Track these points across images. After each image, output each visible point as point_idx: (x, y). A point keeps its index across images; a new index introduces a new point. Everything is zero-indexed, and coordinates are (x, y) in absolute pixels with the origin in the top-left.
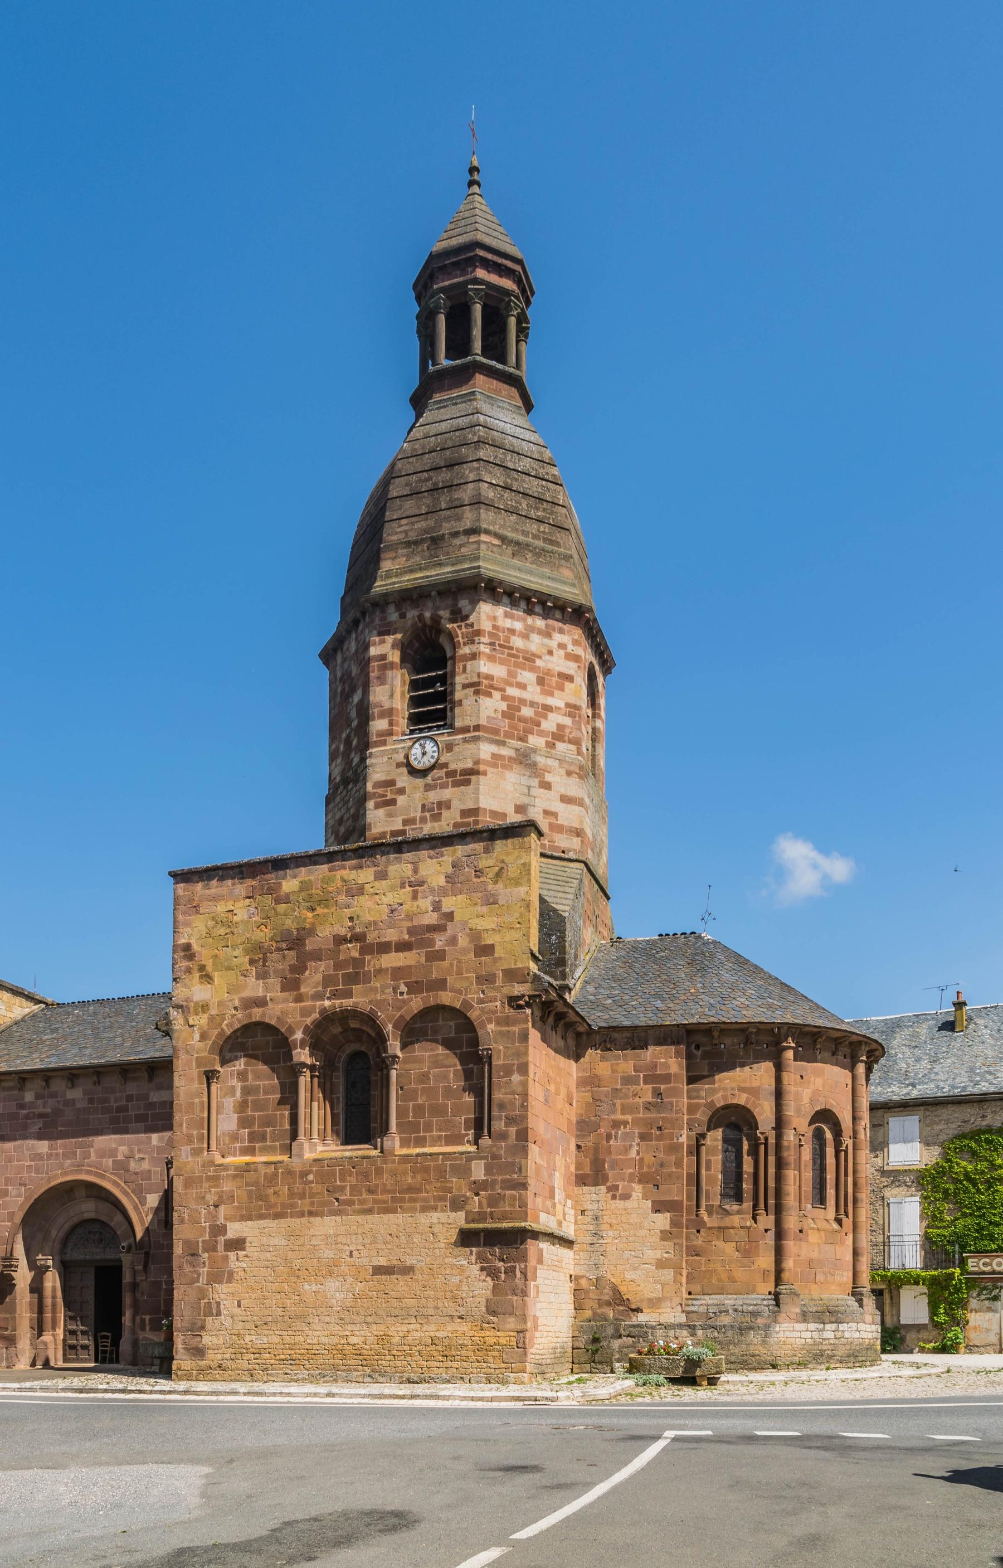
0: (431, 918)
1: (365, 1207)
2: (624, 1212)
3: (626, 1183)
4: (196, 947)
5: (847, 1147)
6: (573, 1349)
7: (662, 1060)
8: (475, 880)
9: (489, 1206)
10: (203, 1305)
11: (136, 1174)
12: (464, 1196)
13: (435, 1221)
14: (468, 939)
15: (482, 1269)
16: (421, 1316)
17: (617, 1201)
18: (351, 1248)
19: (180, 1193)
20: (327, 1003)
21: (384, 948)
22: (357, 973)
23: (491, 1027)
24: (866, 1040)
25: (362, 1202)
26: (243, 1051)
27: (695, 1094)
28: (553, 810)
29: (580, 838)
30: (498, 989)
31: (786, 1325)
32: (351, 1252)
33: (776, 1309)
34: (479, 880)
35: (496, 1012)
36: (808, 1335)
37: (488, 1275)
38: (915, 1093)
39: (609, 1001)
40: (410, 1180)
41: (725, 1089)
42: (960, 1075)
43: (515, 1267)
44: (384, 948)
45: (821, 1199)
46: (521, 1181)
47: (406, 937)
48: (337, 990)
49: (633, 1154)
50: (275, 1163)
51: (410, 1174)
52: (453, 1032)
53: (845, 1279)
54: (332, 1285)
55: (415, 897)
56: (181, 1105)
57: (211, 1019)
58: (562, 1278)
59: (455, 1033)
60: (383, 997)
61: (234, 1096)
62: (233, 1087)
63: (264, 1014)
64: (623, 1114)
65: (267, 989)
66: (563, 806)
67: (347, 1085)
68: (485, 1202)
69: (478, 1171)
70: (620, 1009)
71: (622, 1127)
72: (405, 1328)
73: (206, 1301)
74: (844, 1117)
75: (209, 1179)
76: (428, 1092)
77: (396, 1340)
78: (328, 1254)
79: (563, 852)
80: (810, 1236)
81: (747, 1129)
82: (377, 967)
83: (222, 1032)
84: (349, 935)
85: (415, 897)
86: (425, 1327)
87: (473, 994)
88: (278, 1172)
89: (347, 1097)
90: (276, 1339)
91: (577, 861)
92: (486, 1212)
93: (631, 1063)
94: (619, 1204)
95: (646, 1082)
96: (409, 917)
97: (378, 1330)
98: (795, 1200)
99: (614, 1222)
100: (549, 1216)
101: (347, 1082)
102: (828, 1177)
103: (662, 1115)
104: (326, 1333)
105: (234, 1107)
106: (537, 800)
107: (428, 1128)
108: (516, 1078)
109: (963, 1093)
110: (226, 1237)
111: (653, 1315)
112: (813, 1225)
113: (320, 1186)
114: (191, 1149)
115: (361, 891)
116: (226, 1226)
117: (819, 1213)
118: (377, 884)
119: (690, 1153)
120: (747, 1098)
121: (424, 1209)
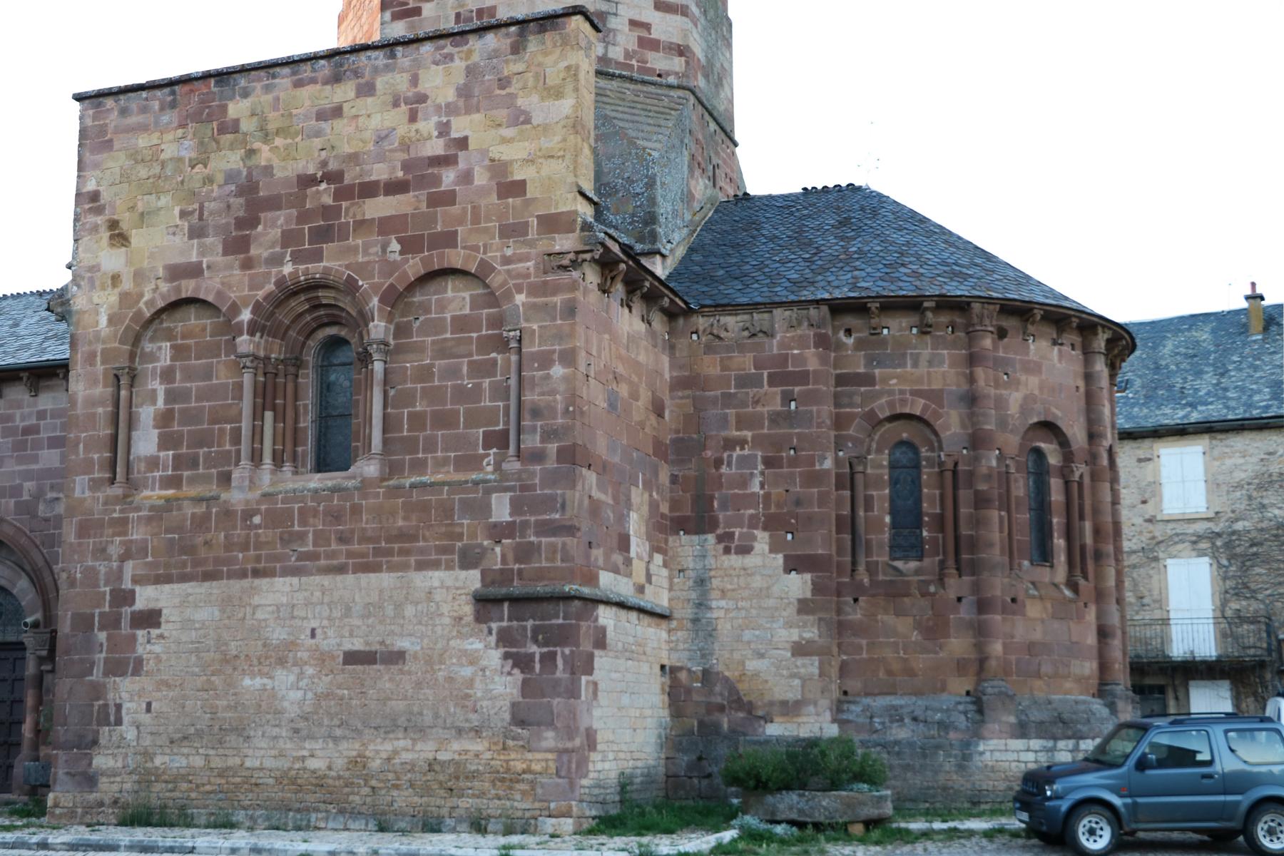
0: (436, 147)
1: (335, 562)
2: (742, 572)
3: (745, 530)
4: (105, 197)
5: (1081, 476)
6: (668, 777)
8: (498, 92)
9: (518, 560)
10: (96, 708)
11: (47, 520)
12: (481, 546)
13: (436, 584)
14: (487, 175)
15: (506, 656)
16: (416, 729)
17: (733, 557)
18: (314, 624)
19: (71, 544)
20: (288, 269)
21: (369, 190)
22: (330, 227)
23: (520, 299)
24: (1101, 322)
25: (332, 555)
27: (846, 400)
28: (644, 19)
29: (683, 59)
30: (531, 244)
31: (995, 742)
32: (313, 630)
33: (978, 717)
34: (503, 92)
35: (528, 276)
36: (1030, 757)
37: (515, 665)
38: (1195, 417)
39: (721, 272)
40: (400, 523)
41: (891, 393)
42: (1259, 392)
43: (555, 653)
44: (369, 190)
45: (1044, 555)
47: (400, 174)
48: (300, 251)
49: (755, 487)
50: (208, 500)
51: (401, 513)
52: (468, 307)
53: (1087, 672)
54: (283, 678)
55: (413, 118)
57: (124, 296)
58: (645, 668)
59: (471, 310)
60: (366, 259)
61: (154, 402)
62: (154, 391)
63: (197, 288)
64: (738, 429)
65: (202, 254)
66: (658, 14)
67: (322, 388)
68: (510, 556)
69: (501, 509)
70: (736, 282)
71: (738, 449)
72: (388, 746)
73: (101, 702)
74: (1074, 434)
77: (376, 764)
78: (278, 634)
79: (659, 76)
80: (1028, 607)
81: (927, 451)
82: (359, 218)
83: (139, 313)
84: (319, 174)
85: (413, 118)
86: (419, 746)
87: (496, 251)
88: (211, 513)
89: (321, 405)
90: (198, 762)
91: (679, 87)
92: (512, 570)
93: (750, 356)
94: (734, 560)
95: (771, 384)
96: (405, 146)
97: (350, 748)
98: (1002, 553)
99: (729, 587)
100: (619, 577)
101: (321, 384)
102: (1055, 520)
103: (796, 431)
104: (273, 752)
106: (620, 6)
107: (430, 446)
108: (558, 371)
109: (1264, 415)
111: (788, 725)
112: (1033, 592)
115: (337, 112)
116: (133, 592)
117: (1044, 574)
118: (360, 102)
119: (839, 486)
120: (925, 405)
121: (421, 566)
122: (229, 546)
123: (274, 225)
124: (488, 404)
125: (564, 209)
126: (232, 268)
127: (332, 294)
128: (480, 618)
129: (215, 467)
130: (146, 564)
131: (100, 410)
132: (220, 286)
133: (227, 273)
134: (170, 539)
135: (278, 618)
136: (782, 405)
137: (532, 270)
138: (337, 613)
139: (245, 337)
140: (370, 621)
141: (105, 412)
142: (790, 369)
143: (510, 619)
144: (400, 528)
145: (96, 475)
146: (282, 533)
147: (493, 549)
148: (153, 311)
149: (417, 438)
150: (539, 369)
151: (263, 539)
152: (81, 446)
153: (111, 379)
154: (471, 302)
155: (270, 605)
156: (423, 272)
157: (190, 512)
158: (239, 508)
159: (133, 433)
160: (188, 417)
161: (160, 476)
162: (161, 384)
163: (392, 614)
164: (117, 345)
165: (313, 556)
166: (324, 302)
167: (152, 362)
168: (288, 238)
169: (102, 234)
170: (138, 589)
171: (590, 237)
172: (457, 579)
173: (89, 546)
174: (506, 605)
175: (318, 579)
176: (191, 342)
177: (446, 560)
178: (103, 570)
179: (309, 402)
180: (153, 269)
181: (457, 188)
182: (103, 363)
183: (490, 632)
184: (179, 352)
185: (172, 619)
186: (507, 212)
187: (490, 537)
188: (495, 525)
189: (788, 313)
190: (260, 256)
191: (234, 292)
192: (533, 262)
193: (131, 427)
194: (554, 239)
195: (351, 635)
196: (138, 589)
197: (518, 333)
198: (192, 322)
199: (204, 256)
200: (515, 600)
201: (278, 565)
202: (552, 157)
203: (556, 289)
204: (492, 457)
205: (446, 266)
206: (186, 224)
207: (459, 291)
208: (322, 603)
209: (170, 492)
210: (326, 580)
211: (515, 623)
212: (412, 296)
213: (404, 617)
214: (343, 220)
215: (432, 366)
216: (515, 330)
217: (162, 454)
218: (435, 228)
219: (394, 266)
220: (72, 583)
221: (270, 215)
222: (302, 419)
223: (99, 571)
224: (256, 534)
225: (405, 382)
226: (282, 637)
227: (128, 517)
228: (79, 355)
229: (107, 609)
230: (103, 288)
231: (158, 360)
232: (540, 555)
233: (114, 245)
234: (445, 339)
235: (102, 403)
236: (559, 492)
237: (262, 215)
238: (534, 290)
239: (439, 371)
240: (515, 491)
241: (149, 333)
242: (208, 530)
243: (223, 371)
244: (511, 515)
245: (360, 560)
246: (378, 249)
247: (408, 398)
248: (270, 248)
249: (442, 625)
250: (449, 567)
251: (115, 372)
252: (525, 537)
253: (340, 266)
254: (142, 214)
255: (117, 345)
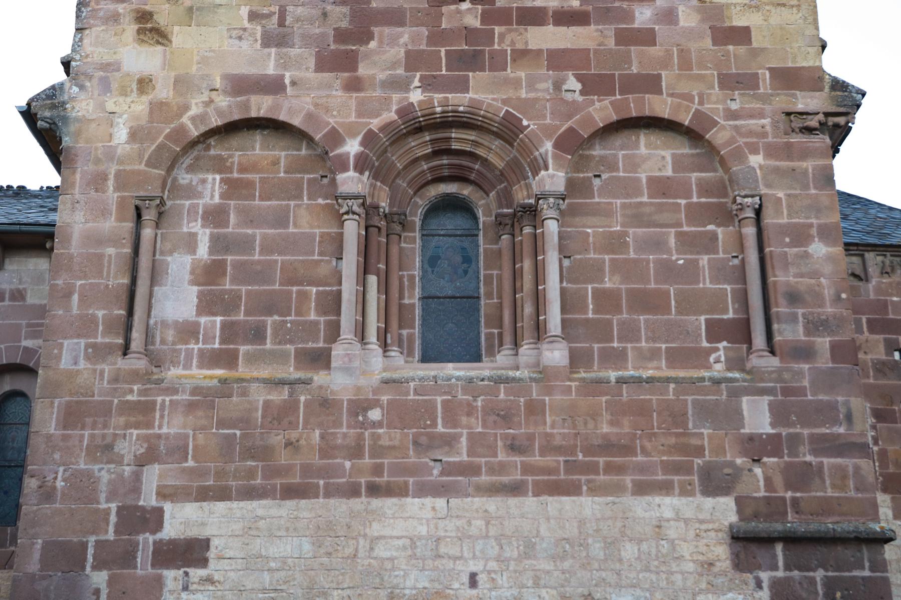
1: (505, 479)
7: (895, 299)
9: (789, 486)
12: (732, 464)
13: (668, 514)
18: (473, 567)
19: (49, 437)
20: (416, 96)
23: (756, 160)
25: (502, 468)
26: (220, 172)
30: (764, 99)
40: (605, 429)
46: (854, 439)
48: (434, 77)
50: (291, 383)
51: (606, 416)
56: (71, 257)
57: (158, 108)
60: (532, 95)
63: (277, 107)
68: (778, 480)
75: (128, 408)
76: (624, 269)
82: (520, 46)
83: (181, 130)
92: (783, 499)
105: (192, 272)
107: (630, 333)
110: (159, 536)
113: (397, 433)
114: (87, 346)
116: (160, 512)
121: (642, 489)
122: (328, 449)
123: (393, 41)
124: (708, 285)
125: (805, 64)
126: (330, 87)
127: (472, 136)
128: (740, 564)
129: (291, 342)
130: (184, 470)
131: (111, 251)
132: (312, 108)
133: (323, 93)
134: (227, 436)
135: (413, 556)
136: (887, 355)
137: (768, 128)
138: (511, 552)
139: (351, 173)
140: (566, 565)
141: (117, 254)
142: (891, 316)
143: (788, 568)
144: (605, 436)
145: (100, 340)
146: (415, 436)
147: (750, 470)
148: (203, 129)
149: (609, 323)
150: (792, 245)
151: (385, 442)
152: (76, 297)
153: (132, 212)
154: (674, 163)
155: (398, 538)
156: (614, 118)
157: (261, 400)
158: (345, 397)
159: (156, 288)
160: (245, 273)
161: (199, 349)
162: (203, 226)
163: (601, 555)
164: (142, 167)
165: (470, 470)
166: (455, 146)
167: (189, 198)
168: (413, 60)
169: (125, 27)
170: (168, 507)
171: (844, 98)
172: (699, 508)
173: (81, 441)
174: (779, 548)
175: (478, 502)
176: (255, 177)
177: (679, 481)
178: (105, 477)
179: (417, 273)
180: (205, 77)
181: (657, 27)
182: (117, 189)
183: (759, 585)
184: (233, 188)
185: (229, 553)
186: (729, 60)
187: (744, 453)
188: (751, 438)
189: (880, 258)
190: (373, 77)
191: (335, 117)
192: (769, 120)
193: (154, 279)
194: (794, 96)
195: (536, 585)
196: (168, 507)
197: (757, 199)
198: (257, 152)
199: (286, 69)
200: (791, 540)
201: (411, 480)
202: (784, 5)
203: (805, 154)
204: (721, 353)
205: (647, 113)
206: (259, 28)
207: (656, 148)
208: (487, 537)
209: (219, 372)
210: (493, 504)
211: (796, 573)
212: (589, 149)
213: (620, 560)
214: (496, 47)
215: (626, 234)
216: (752, 196)
217: (203, 320)
218: (629, 68)
219: (572, 109)
220: (48, 494)
221: (387, 30)
222: (406, 295)
223: (99, 478)
224: (373, 434)
225: (587, 250)
226: (420, 585)
227: (154, 403)
228: (78, 176)
229: (111, 536)
230: (124, 93)
231: (199, 195)
232: (823, 481)
233: (143, 41)
234: (641, 203)
235: (114, 241)
236: (840, 399)
237: (376, 30)
238: (771, 152)
239: (635, 241)
240: (776, 396)
241: (188, 161)
242: (293, 425)
243: (305, 217)
244: (773, 425)
245: (546, 478)
246: (549, 85)
247: (595, 272)
248: (389, 69)
249: (682, 573)
250: (686, 492)
251: (138, 202)
252: (797, 456)
253: (493, 99)
254: (190, 9)
255: (142, 167)
